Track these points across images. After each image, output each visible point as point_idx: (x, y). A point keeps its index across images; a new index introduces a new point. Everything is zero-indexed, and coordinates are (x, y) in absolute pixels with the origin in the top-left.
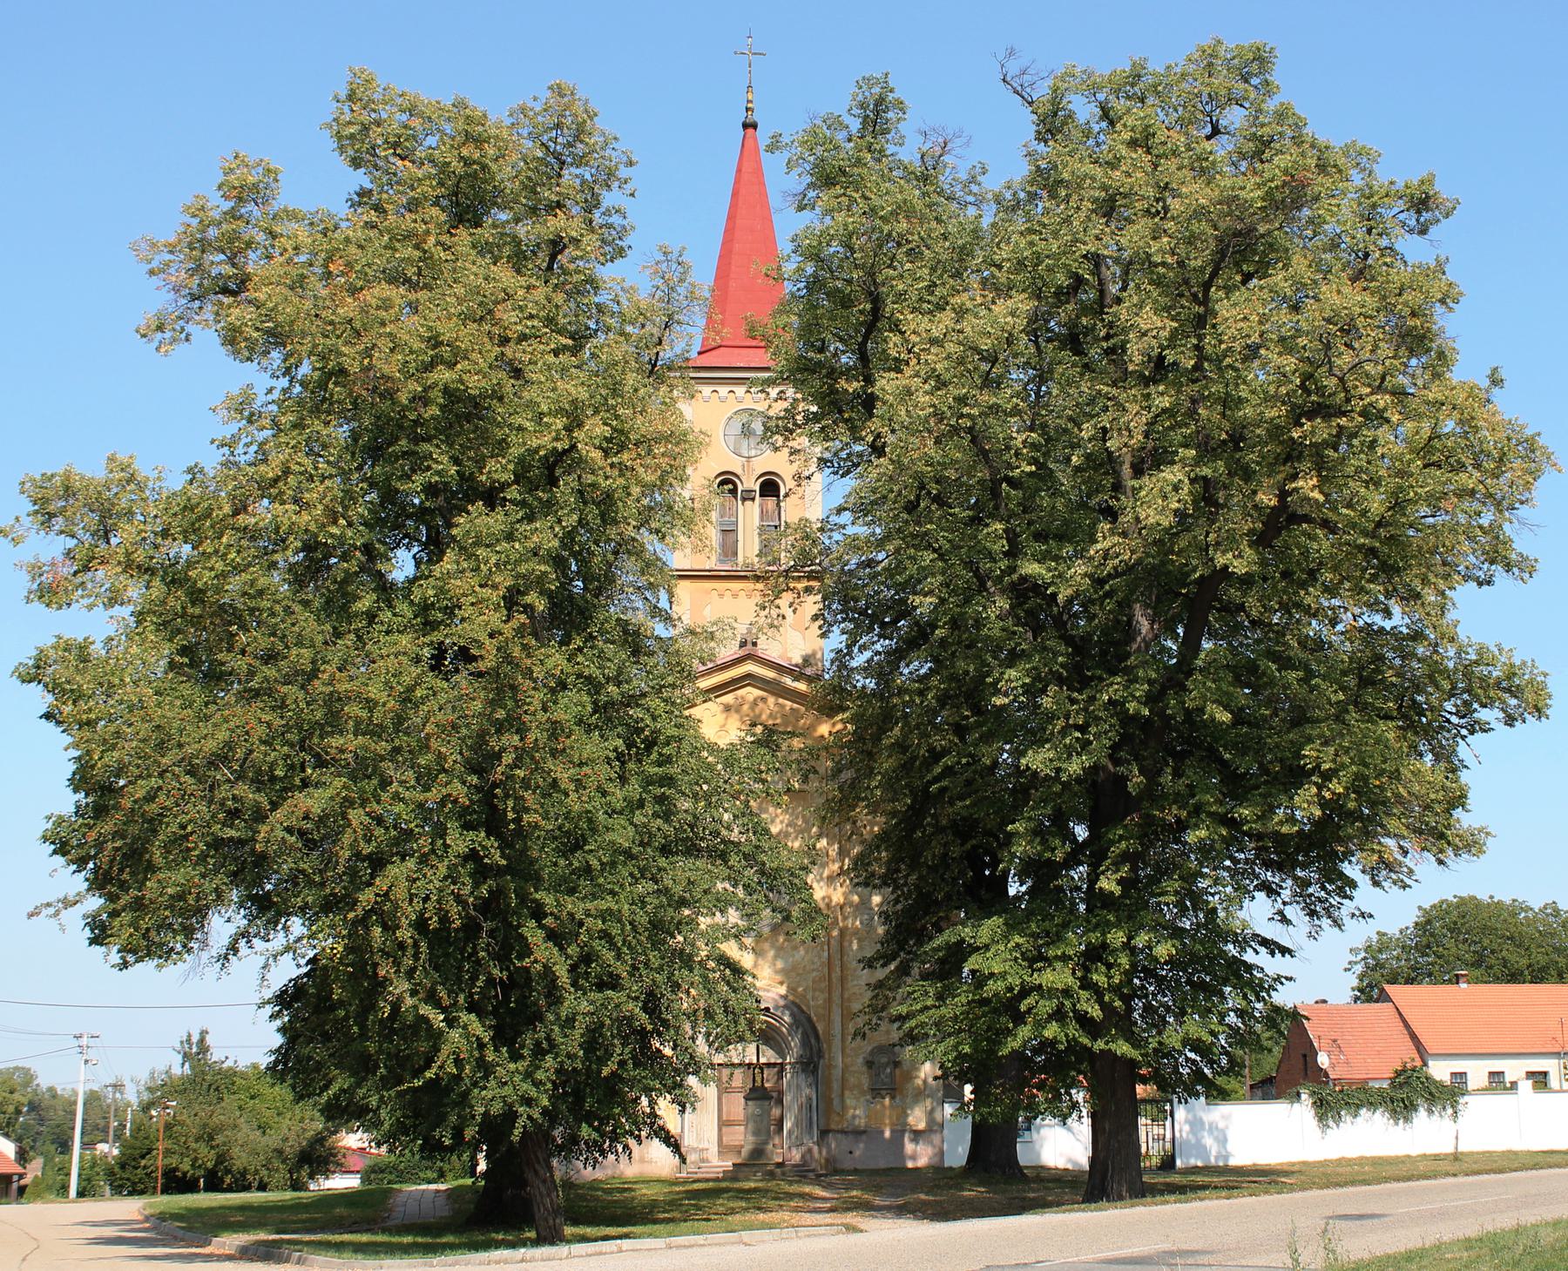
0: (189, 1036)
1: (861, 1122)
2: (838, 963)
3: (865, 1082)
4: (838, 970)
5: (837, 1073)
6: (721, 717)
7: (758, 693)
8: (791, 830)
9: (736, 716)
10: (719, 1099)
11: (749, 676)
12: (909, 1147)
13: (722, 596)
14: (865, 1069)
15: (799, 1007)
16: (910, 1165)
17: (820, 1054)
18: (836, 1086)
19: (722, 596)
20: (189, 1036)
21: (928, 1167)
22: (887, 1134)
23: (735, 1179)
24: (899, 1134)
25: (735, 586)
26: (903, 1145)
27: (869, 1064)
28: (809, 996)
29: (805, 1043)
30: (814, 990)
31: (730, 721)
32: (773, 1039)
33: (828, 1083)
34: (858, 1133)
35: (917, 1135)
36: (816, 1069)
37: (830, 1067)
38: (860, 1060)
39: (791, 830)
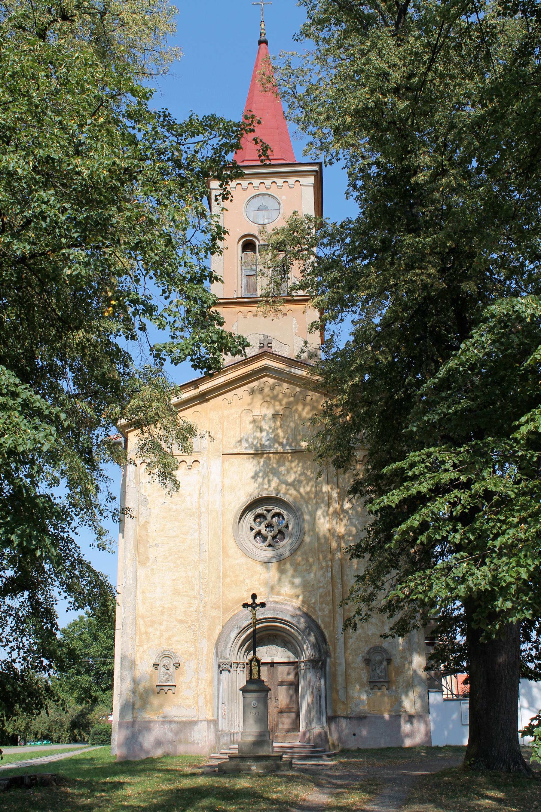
0: (167, 474)
1: (364, 708)
2: (339, 581)
3: (364, 677)
4: (340, 587)
5: (341, 669)
6: (247, 398)
7: (271, 381)
8: (302, 478)
9: (260, 397)
11: (265, 369)
12: (406, 728)
13: (245, 316)
14: (363, 666)
15: (310, 617)
16: (408, 743)
17: (327, 654)
18: (340, 679)
19: (245, 316)
20: (167, 474)
21: (421, 746)
22: (386, 716)
23: (237, 772)
24: (396, 717)
25: (245, 309)
26: (399, 726)
27: (367, 661)
28: (318, 608)
29: (317, 646)
30: (322, 603)
31: (255, 400)
32: (290, 642)
33: (334, 675)
34: (361, 718)
35: (411, 718)
36: (324, 664)
37: (334, 664)
38: (360, 659)
39: (302, 478)
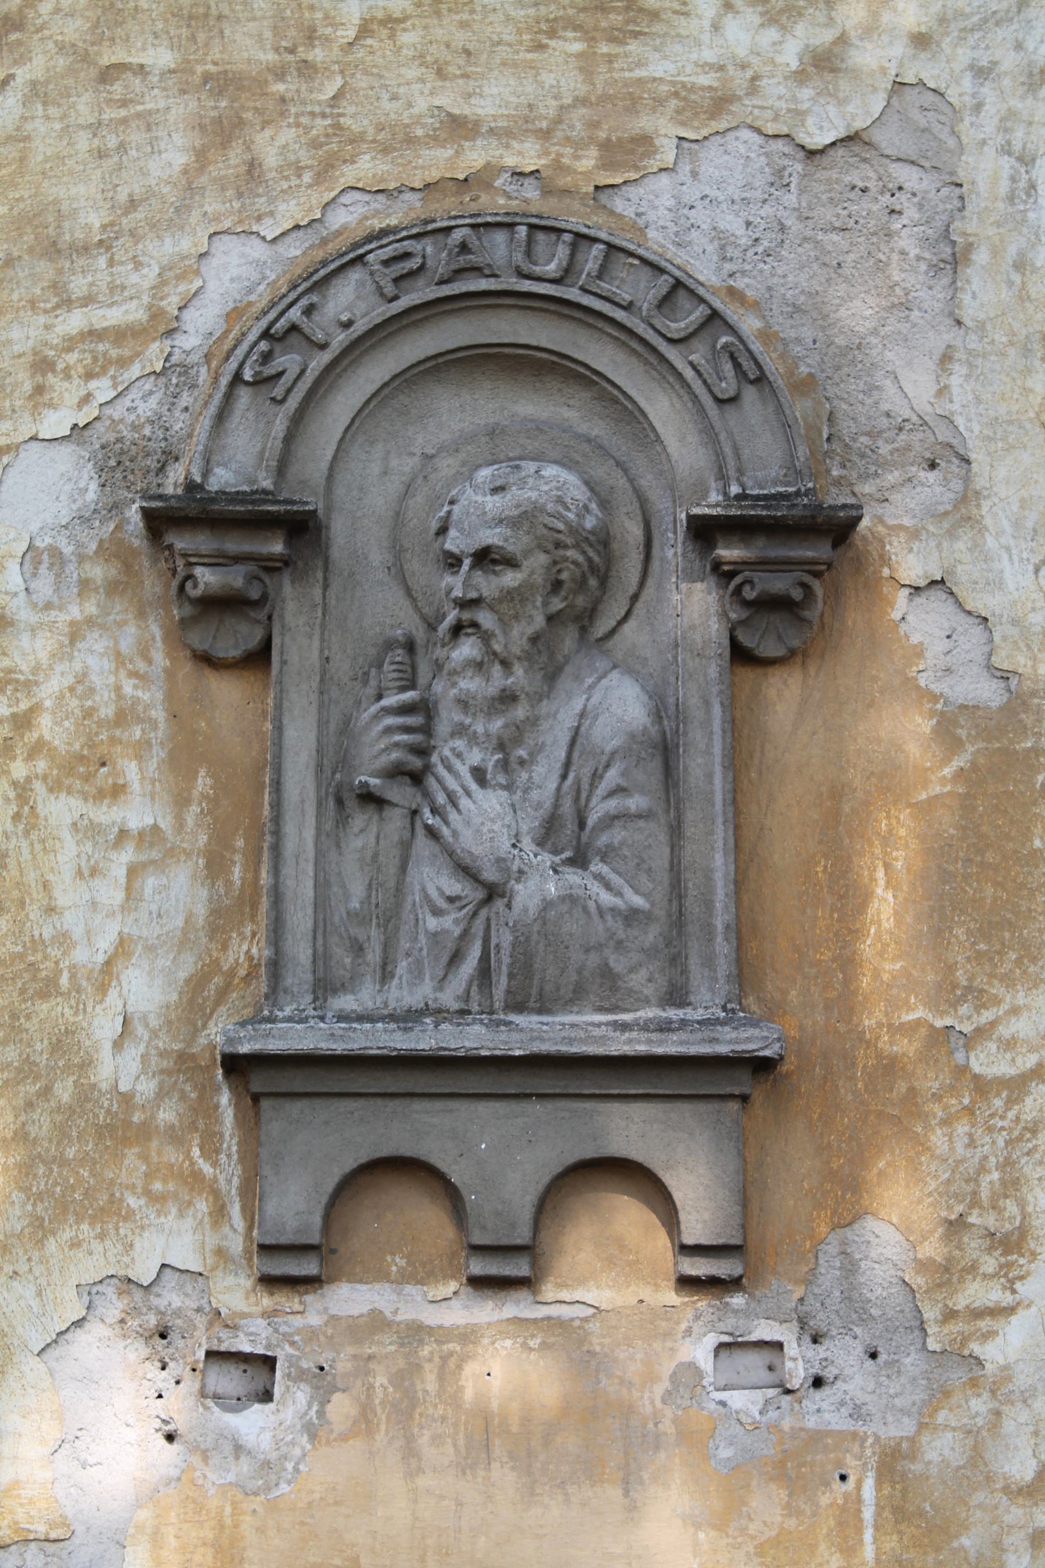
10: (759, 366)
27: (224, 559)
